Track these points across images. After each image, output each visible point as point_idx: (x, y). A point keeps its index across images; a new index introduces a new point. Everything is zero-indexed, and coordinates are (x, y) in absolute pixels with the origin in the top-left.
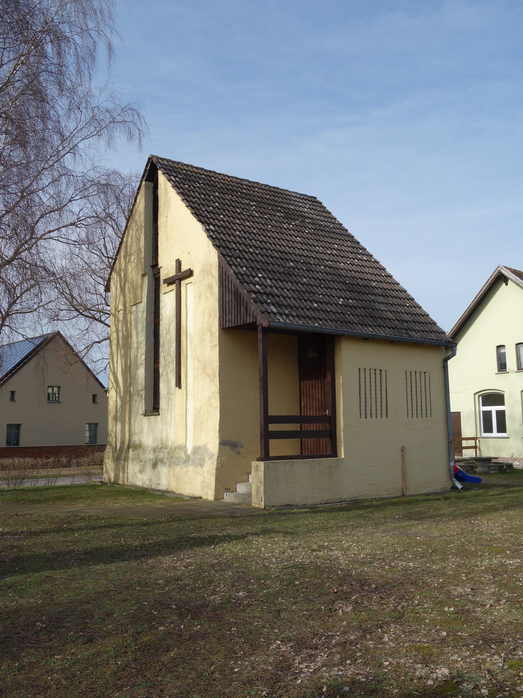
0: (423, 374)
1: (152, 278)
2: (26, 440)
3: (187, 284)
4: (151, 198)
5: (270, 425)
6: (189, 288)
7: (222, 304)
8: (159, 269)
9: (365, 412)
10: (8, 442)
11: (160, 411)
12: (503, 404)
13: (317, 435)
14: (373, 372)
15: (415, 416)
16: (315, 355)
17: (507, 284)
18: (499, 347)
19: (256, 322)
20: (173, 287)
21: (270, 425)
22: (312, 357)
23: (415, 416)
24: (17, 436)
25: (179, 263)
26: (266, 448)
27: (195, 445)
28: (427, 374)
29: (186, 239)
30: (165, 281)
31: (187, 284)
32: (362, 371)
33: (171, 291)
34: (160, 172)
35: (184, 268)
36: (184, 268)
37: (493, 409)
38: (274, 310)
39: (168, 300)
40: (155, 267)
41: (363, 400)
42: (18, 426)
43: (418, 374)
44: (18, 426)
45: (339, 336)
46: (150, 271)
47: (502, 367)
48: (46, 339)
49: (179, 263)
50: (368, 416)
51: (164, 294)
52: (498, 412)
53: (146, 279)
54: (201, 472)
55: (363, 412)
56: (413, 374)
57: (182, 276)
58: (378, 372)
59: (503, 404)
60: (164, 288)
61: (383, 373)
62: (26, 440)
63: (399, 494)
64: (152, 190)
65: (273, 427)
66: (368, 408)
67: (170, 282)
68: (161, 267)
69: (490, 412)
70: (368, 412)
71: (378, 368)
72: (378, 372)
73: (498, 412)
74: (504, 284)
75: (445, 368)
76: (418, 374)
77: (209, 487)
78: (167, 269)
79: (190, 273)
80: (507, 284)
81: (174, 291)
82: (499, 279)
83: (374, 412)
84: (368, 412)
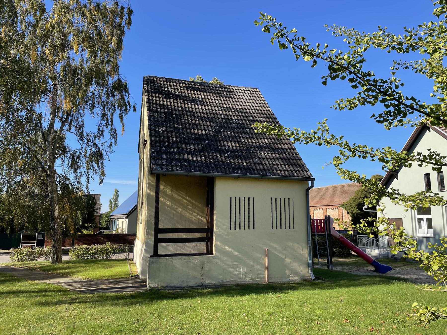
17: (430, 131)
70: (238, 225)
84: (238, 225)
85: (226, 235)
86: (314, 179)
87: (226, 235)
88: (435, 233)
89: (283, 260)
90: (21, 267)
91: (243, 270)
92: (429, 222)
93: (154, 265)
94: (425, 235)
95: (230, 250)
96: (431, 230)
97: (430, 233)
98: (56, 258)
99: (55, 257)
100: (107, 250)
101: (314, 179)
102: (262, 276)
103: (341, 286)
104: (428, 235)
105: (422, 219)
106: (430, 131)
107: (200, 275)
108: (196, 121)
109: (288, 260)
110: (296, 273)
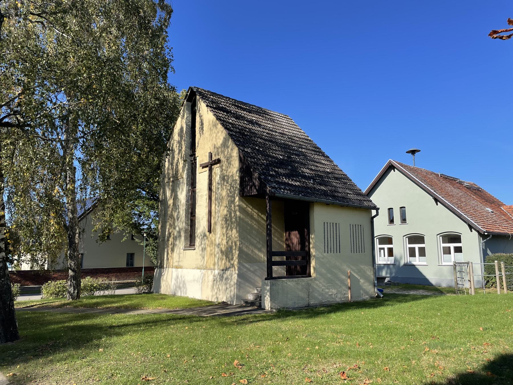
0: (359, 226)
12: (423, 242)
13: (298, 265)
15: (332, 251)
17: (394, 171)
18: (389, 209)
22: (295, 216)
23: (332, 251)
29: (212, 135)
30: (201, 165)
37: (417, 246)
45: (313, 202)
47: (392, 221)
50: (329, 252)
52: (420, 248)
55: (326, 250)
56: (354, 226)
59: (423, 242)
60: (199, 169)
69: (414, 248)
70: (329, 250)
71: (357, 224)
73: (420, 248)
75: (372, 223)
81: (208, 171)
82: (391, 167)
84: (329, 250)
85: (323, 258)
86: (379, 209)
87: (323, 258)
88: (395, 260)
89: (359, 281)
90: (43, 304)
91: (334, 291)
92: (391, 252)
93: (274, 287)
94: (385, 263)
95: (325, 272)
96: (392, 259)
97: (391, 260)
98: (77, 293)
99: (76, 292)
100: (92, 285)
101: (379, 209)
102: (347, 296)
103: (350, 310)
104: (389, 263)
105: (383, 249)
106: (394, 171)
107: (306, 296)
108: (125, 176)
109: (362, 281)
110: (367, 293)
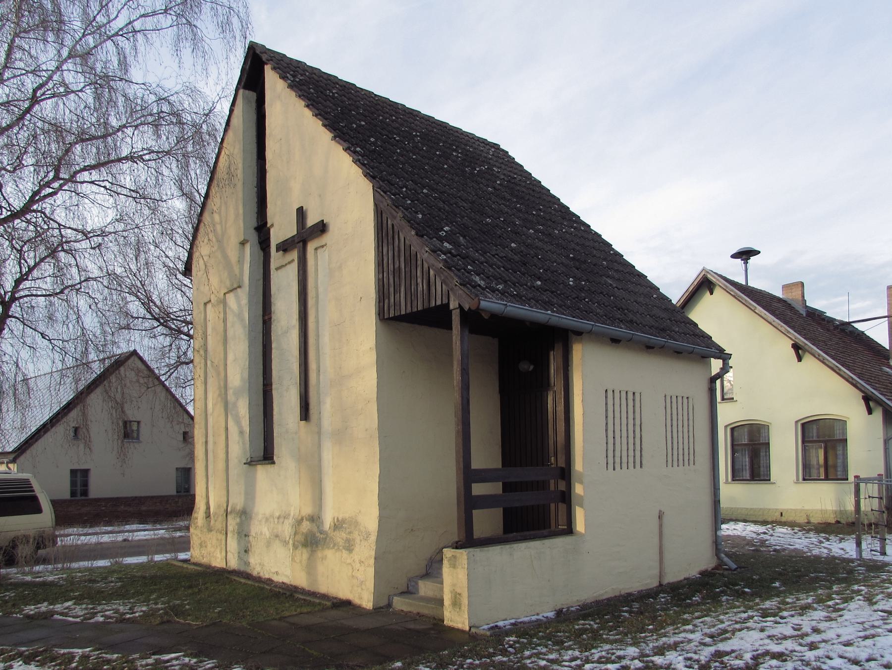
0: (685, 400)
1: (257, 248)
2: (98, 488)
3: (316, 249)
4: (254, 117)
5: (473, 485)
6: (319, 258)
7: (381, 276)
8: (269, 230)
9: (613, 462)
10: (73, 494)
11: (275, 458)
14: (623, 394)
16: (532, 367)
17: (712, 293)
19: (448, 304)
20: (294, 255)
21: (473, 485)
24: (85, 484)
25: (301, 213)
26: (467, 524)
27: (336, 515)
28: (690, 400)
31: (316, 249)
32: (610, 393)
33: (289, 263)
34: (268, 69)
35: (311, 221)
36: (311, 221)
38: (482, 283)
39: (284, 281)
40: (262, 230)
41: (611, 441)
42: (85, 472)
43: (680, 399)
44: (85, 472)
46: (254, 237)
48: (116, 362)
49: (301, 213)
51: (277, 269)
53: (248, 247)
54: (349, 561)
57: (309, 233)
58: (630, 396)
60: (276, 258)
61: (637, 396)
62: (98, 488)
63: (658, 584)
64: (254, 105)
65: (478, 489)
66: (618, 454)
67: (284, 247)
68: (272, 225)
72: (630, 396)
74: (708, 293)
76: (680, 399)
77: (364, 587)
78: (282, 228)
79: (322, 228)
80: (712, 293)
83: (624, 459)
